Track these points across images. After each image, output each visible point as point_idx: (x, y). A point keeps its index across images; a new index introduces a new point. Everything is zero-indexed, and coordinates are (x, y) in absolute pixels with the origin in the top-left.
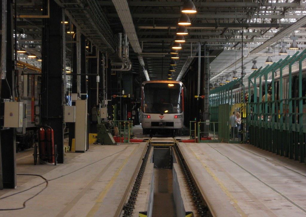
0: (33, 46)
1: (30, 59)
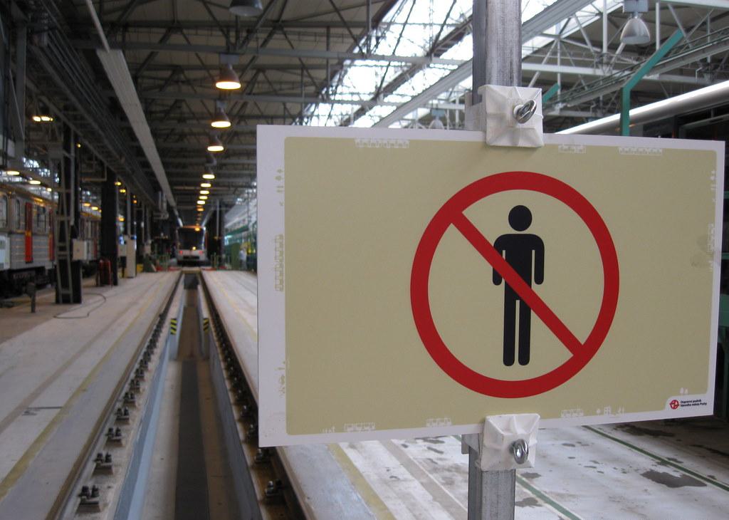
0: (94, 201)
1: (92, 209)
